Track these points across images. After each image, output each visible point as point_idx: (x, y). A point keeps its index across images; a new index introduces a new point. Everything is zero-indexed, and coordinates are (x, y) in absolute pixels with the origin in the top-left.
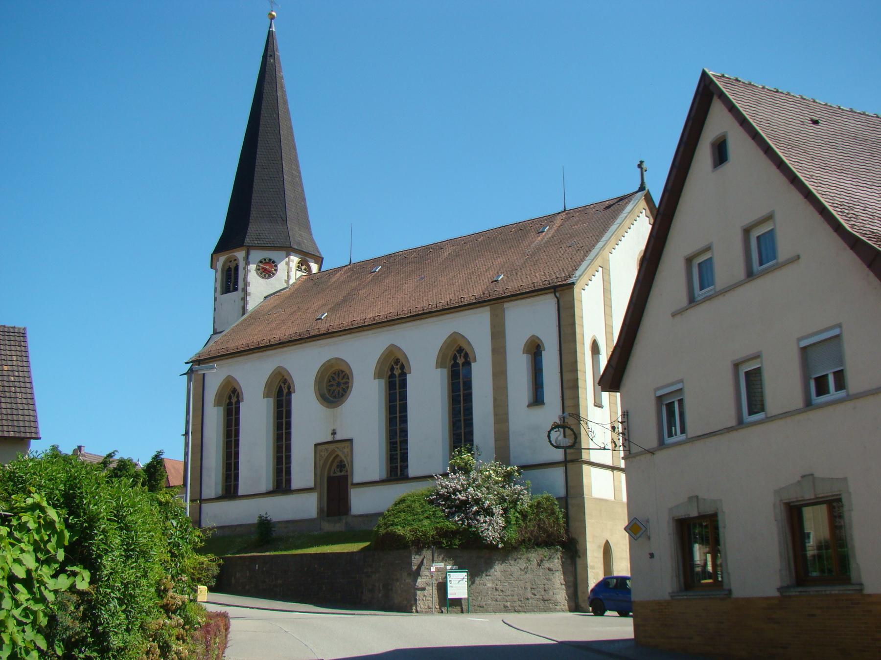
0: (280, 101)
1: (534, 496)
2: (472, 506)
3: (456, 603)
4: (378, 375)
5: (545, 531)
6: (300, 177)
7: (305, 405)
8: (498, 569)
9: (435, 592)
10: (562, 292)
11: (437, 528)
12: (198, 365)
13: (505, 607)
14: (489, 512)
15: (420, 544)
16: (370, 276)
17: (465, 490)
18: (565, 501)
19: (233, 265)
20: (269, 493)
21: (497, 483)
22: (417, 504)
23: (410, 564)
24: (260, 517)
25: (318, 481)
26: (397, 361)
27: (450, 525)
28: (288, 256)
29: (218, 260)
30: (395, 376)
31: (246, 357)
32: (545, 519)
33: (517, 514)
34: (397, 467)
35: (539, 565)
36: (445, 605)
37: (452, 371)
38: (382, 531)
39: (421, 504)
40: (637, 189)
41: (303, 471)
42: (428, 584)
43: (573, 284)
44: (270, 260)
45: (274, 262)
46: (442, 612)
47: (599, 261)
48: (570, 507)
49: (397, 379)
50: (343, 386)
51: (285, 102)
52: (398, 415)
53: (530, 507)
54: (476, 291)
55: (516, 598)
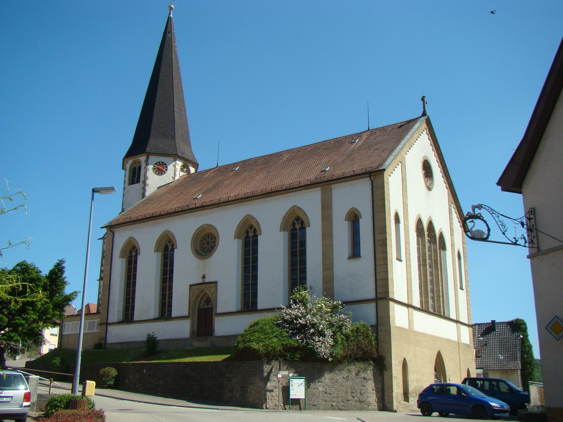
0: (174, 61)
1: (354, 324)
2: (310, 329)
3: (296, 402)
4: (238, 236)
5: (362, 349)
6: (185, 111)
7: (184, 256)
8: (327, 377)
9: (281, 394)
10: (375, 176)
11: (283, 344)
12: (111, 228)
13: (332, 406)
14: (321, 334)
15: (270, 356)
16: (231, 173)
17: (305, 317)
18: (376, 328)
19: (137, 166)
20: (155, 320)
21: (326, 313)
22: (268, 327)
23: (262, 371)
24: (149, 335)
25: (191, 311)
26: (251, 227)
27: (293, 343)
28: (175, 161)
29: (127, 163)
30: (249, 237)
31: (142, 224)
32: (362, 341)
33: (342, 336)
34: (249, 302)
35: (357, 375)
36: (288, 404)
37: (292, 234)
38: (241, 346)
39: (271, 326)
40: (421, 115)
41: (181, 303)
42: (275, 387)
43: (384, 170)
44: (163, 163)
45: (165, 164)
46: (285, 409)
47: (399, 158)
48: (379, 333)
49: (251, 239)
50: (211, 244)
51: (177, 62)
52: (251, 265)
53: (352, 331)
54: (311, 176)
55: (340, 399)
